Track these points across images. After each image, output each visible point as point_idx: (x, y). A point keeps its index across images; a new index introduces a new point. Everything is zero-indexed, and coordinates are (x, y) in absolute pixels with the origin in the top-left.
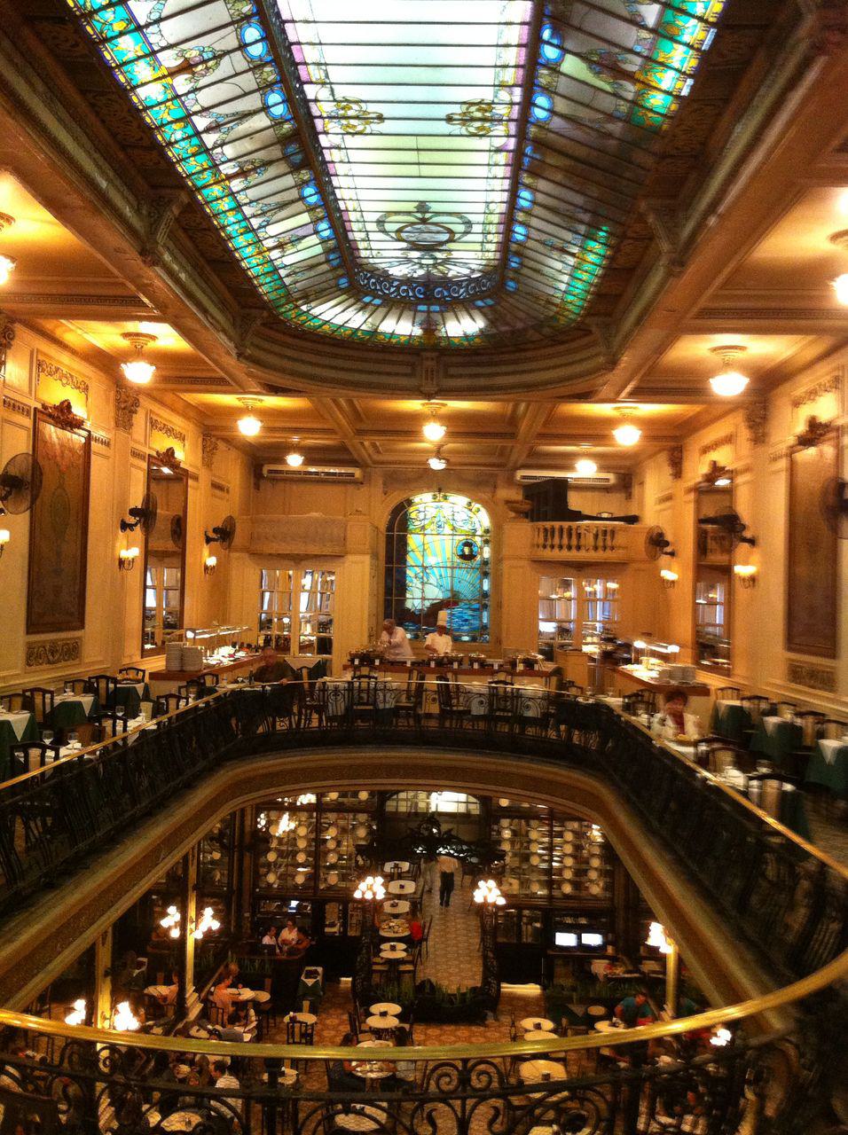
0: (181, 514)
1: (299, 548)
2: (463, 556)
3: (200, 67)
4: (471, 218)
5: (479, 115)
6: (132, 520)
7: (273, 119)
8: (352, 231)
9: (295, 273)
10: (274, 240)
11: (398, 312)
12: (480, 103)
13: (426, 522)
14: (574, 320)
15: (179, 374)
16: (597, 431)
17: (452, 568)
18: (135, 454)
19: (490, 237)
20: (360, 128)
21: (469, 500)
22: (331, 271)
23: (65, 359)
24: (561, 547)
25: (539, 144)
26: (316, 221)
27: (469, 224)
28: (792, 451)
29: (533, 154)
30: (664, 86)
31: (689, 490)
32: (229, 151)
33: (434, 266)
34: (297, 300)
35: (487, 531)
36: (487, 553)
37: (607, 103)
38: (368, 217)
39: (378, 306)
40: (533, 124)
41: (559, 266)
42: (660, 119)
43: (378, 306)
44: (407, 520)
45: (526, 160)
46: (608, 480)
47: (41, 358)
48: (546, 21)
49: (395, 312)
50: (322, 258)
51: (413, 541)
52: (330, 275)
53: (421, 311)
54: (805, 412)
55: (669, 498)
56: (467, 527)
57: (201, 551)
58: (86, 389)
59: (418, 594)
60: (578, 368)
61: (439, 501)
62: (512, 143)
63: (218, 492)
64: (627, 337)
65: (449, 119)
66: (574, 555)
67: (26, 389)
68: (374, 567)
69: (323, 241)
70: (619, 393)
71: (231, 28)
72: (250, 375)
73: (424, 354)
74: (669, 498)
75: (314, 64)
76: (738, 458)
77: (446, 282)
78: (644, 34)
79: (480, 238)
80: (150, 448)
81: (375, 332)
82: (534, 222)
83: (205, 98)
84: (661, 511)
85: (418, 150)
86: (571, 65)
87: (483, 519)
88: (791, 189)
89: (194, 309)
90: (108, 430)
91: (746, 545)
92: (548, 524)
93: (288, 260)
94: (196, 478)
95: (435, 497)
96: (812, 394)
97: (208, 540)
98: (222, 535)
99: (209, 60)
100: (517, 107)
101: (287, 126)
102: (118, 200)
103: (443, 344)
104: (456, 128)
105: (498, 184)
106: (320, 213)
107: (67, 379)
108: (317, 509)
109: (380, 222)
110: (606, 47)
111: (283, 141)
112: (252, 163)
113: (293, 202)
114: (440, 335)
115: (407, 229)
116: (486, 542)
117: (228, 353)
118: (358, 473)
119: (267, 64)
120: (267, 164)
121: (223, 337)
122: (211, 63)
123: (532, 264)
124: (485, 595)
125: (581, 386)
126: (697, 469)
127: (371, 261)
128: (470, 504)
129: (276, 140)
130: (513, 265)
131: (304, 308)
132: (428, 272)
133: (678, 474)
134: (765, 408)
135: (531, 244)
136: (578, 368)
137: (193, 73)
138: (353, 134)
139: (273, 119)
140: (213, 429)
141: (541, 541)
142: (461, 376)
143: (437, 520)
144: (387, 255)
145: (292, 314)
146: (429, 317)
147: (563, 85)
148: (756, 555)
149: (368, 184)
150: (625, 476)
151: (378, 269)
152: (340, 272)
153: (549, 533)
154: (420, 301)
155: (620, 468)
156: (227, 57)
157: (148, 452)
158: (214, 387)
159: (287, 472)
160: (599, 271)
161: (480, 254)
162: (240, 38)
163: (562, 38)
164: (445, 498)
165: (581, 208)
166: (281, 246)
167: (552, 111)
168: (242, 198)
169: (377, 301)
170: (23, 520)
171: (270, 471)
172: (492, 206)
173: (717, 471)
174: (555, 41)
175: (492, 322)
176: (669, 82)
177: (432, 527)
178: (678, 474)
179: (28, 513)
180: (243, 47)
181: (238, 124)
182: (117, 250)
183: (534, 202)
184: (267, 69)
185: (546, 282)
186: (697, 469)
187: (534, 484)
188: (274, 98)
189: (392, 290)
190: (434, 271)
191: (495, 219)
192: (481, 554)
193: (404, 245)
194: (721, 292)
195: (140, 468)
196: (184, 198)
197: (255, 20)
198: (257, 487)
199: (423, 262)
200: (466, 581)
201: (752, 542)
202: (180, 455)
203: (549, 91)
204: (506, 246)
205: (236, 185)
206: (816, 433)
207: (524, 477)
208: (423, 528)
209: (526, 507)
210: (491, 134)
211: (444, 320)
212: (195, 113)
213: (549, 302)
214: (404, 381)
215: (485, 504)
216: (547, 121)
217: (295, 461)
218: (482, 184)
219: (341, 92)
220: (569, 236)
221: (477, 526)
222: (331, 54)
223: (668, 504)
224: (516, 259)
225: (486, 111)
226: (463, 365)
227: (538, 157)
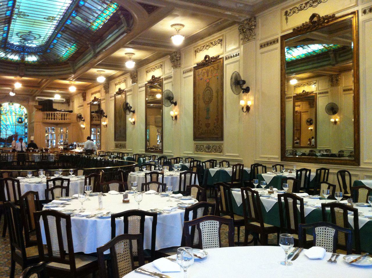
2: (19, 122)
17: (16, 125)
20: (22, 17)
21: (20, 105)
27: (40, 37)
31: (88, 104)
35: (26, 114)
36: (26, 121)
37: (85, 25)
39: (10, 52)
41: (64, 49)
46: (63, 100)
49: (14, 54)
54: (118, 87)
55: (82, 106)
56: (20, 113)
59: (4, 133)
60: (65, 72)
64: (79, 67)
66: (53, 121)
69: (3, 37)
73: (20, 65)
74: (82, 106)
76: (101, 96)
81: (7, 58)
87: (25, 111)
91: (104, 117)
92: (48, 112)
96: (120, 83)
103: (26, 63)
116: (26, 118)
123: (55, 47)
125: (64, 77)
126: (90, 98)
128: (20, 106)
133: (85, 99)
134: (109, 85)
136: (65, 72)
141: (46, 117)
143: (10, 111)
148: (107, 120)
150: (68, 99)
164: (13, 104)
169: (10, 51)
173: (96, 99)
177: (9, 113)
178: (85, 99)
186: (90, 98)
187: (42, 101)
192: (25, 121)
193: (21, 39)
201: (106, 117)
206: (120, 92)
207: (38, 99)
208: (6, 113)
209: (40, 107)
214: (13, 72)
215: (25, 106)
216: (69, 24)
219: (20, 10)
221: (23, 113)
223: (82, 107)
226: (32, 68)
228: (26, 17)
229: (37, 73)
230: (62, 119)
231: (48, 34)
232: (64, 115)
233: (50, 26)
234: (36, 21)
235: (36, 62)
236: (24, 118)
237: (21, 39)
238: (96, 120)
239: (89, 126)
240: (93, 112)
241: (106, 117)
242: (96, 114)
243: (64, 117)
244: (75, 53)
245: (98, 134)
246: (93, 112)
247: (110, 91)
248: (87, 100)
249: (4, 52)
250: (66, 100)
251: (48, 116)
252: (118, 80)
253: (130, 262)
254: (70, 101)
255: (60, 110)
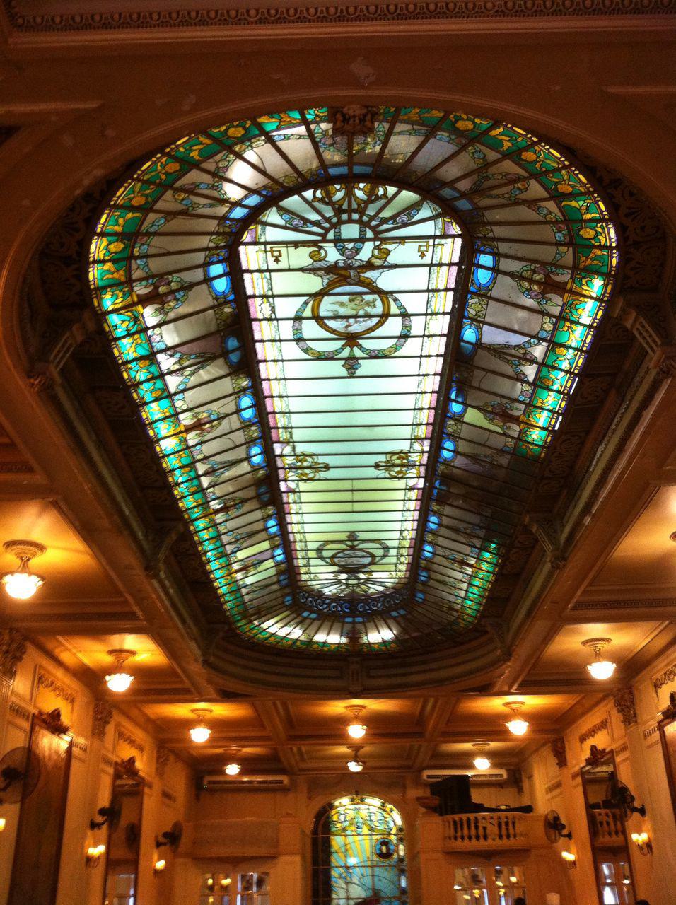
0: (136, 822)
1: (238, 851)
2: (381, 855)
3: (208, 426)
4: (389, 543)
5: (398, 462)
6: (99, 819)
7: (253, 466)
8: (297, 559)
9: (253, 592)
10: (240, 569)
11: (329, 624)
12: (400, 453)
13: (347, 823)
14: (472, 623)
15: (153, 685)
16: (492, 727)
17: (372, 867)
18: (106, 761)
19: (403, 559)
20: (311, 476)
21: (382, 801)
22: (279, 590)
23: (59, 674)
24: (470, 838)
25: (447, 479)
26: (273, 548)
27: (386, 548)
28: (661, 726)
29: (441, 488)
30: (541, 424)
31: (574, 776)
32: (218, 491)
33: (358, 585)
34: (252, 615)
35: (400, 830)
36: (402, 850)
37: (499, 442)
38: (310, 546)
39: (314, 620)
40: (441, 463)
41: (460, 576)
42: (539, 449)
43: (314, 620)
44: (330, 823)
45: (435, 492)
46: (501, 776)
47: (42, 672)
48: (454, 385)
49: (327, 624)
50: (275, 579)
51: (337, 842)
52: (279, 594)
53: (347, 623)
55: (558, 785)
57: (152, 855)
58: (72, 701)
60: (474, 665)
61: (358, 804)
62: (421, 483)
63: (167, 801)
65: (377, 466)
66: (482, 845)
67: (28, 697)
68: (304, 870)
69: (277, 565)
70: (510, 687)
71: (233, 397)
72: (209, 682)
74: (558, 785)
75: (283, 428)
77: (367, 598)
78: (526, 387)
79: (394, 560)
80: (117, 756)
81: (310, 642)
82: (441, 541)
83: (207, 449)
84: (553, 798)
85: (352, 491)
86: (472, 416)
87: (396, 818)
88: (637, 501)
89: (176, 619)
90: (86, 738)
91: (636, 815)
92: (457, 817)
93: (249, 581)
94: (150, 786)
95: (353, 800)
97: (158, 845)
98: (170, 840)
99: (215, 420)
100: (426, 455)
101: (261, 472)
102: (135, 525)
104: (381, 473)
105: (410, 515)
106: (278, 541)
107: (60, 691)
108: (250, 815)
109: (319, 550)
110: (498, 400)
111: (258, 483)
112: (234, 501)
113: (258, 532)
114: (363, 642)
115: (340, 555)
117: (196, 660)
118: (285, 779)
119: (254, 424)
120: (243, 501)
121: (195, 645)
122: (215, 423)
124: (403, 892)
125: (479, 680)
126: (579, 756)
127: (309, 583)
128: (383, 805)
129: (252, 483)
130: (422, 578)
131: (256, 623)
132: (353, 590)
133: (562, 762)
134: (631, 693)
135: (437, 559)
137: (202, 430)
138: (305, 481)
139: (253, 466)
140: (167, 739)
142: (380, 677)
144: (322, 577)
145: (246, 628)
146: (354, 627)
147: (465, 431)
149: (311, 519)
151: (313, 590)
152: (287, 591)
153: (457, 825)
154: (348, 615)
155: (510, 764)
156: (227, 419)
157: (115, 759)
158: (177, 697)
159: (226, 782)
160: (491, 577)
161: (394, 573)
162: (238, 405)
163: (465, 398)
164: (362, 801)
165: (478, 526)
166: (245, 569)
167: (456, 452)
168: (222, 528)
169: (313, 616)
170: (14, 809)
171: (210, 782)
172: (405, 534)
173: (597, 757)
174: (460, 400)
175: (404, 630)
176: (542, 424)
177: (352, 828)
178: (562, 762)
179: (18, 805)
180: (239, 411)
181: (228, 470)
182: (128, 567)
183: (440, 525)
184: (253, 428)
185: (448, 590)
186: (579, 756)
187: (439, 782)
188: (255, 450)
189: (325, 606)
190: (358, 590)
191: (407, 544)
192: (397, 851)
193: (335, 568)
194: (589, 588)
195: (107, 773)
196: (181, 528)
197: (249, 392)
198: (197, 798)
199: (350, 582)
200: (386, 881)
201: (642, 811)
202: (139, 765)
203: (454, 437)
204: (414, 567)
205: (219, 518)
207: (429, 777)
208: (344, 830)
209: (435, 802)
210: (407, 476)
211: (366, 630)
212: (199, 461)
213: (451, 609)
214: (333, 683)
216: (451, 460)
217: (232, 770)
218: (398, 516)
219: (300, 448)
220: (468, 550)
221: (392, 825)
222: (296, 420)
224: (424, 574)
225: (404, 459)
227: (444, 488)
228: (323, 474)
229: (399, 680)
230: (501, 837)
231: (405, 534)
232: (507, 824)
233: (400, 495)
234: (358, 485)
235: (391, 642)
236: (395, 842)
237: (335, 568)
238: (610, 834)
239: (590, 855)
240: (597, 806)
241: (642, 811)
242: (607, 811)
243: (507, 829)
244: (496, 580)
245: (627, 882)
246: (597, 806)
247: (637, 712)
248: (568, 763)
249: (297, 620)
250: (508, 774)
251: (459, 829)
252: (663, 664)
253: (433, 383)
254: (521, 778)
255: (494, 807)
